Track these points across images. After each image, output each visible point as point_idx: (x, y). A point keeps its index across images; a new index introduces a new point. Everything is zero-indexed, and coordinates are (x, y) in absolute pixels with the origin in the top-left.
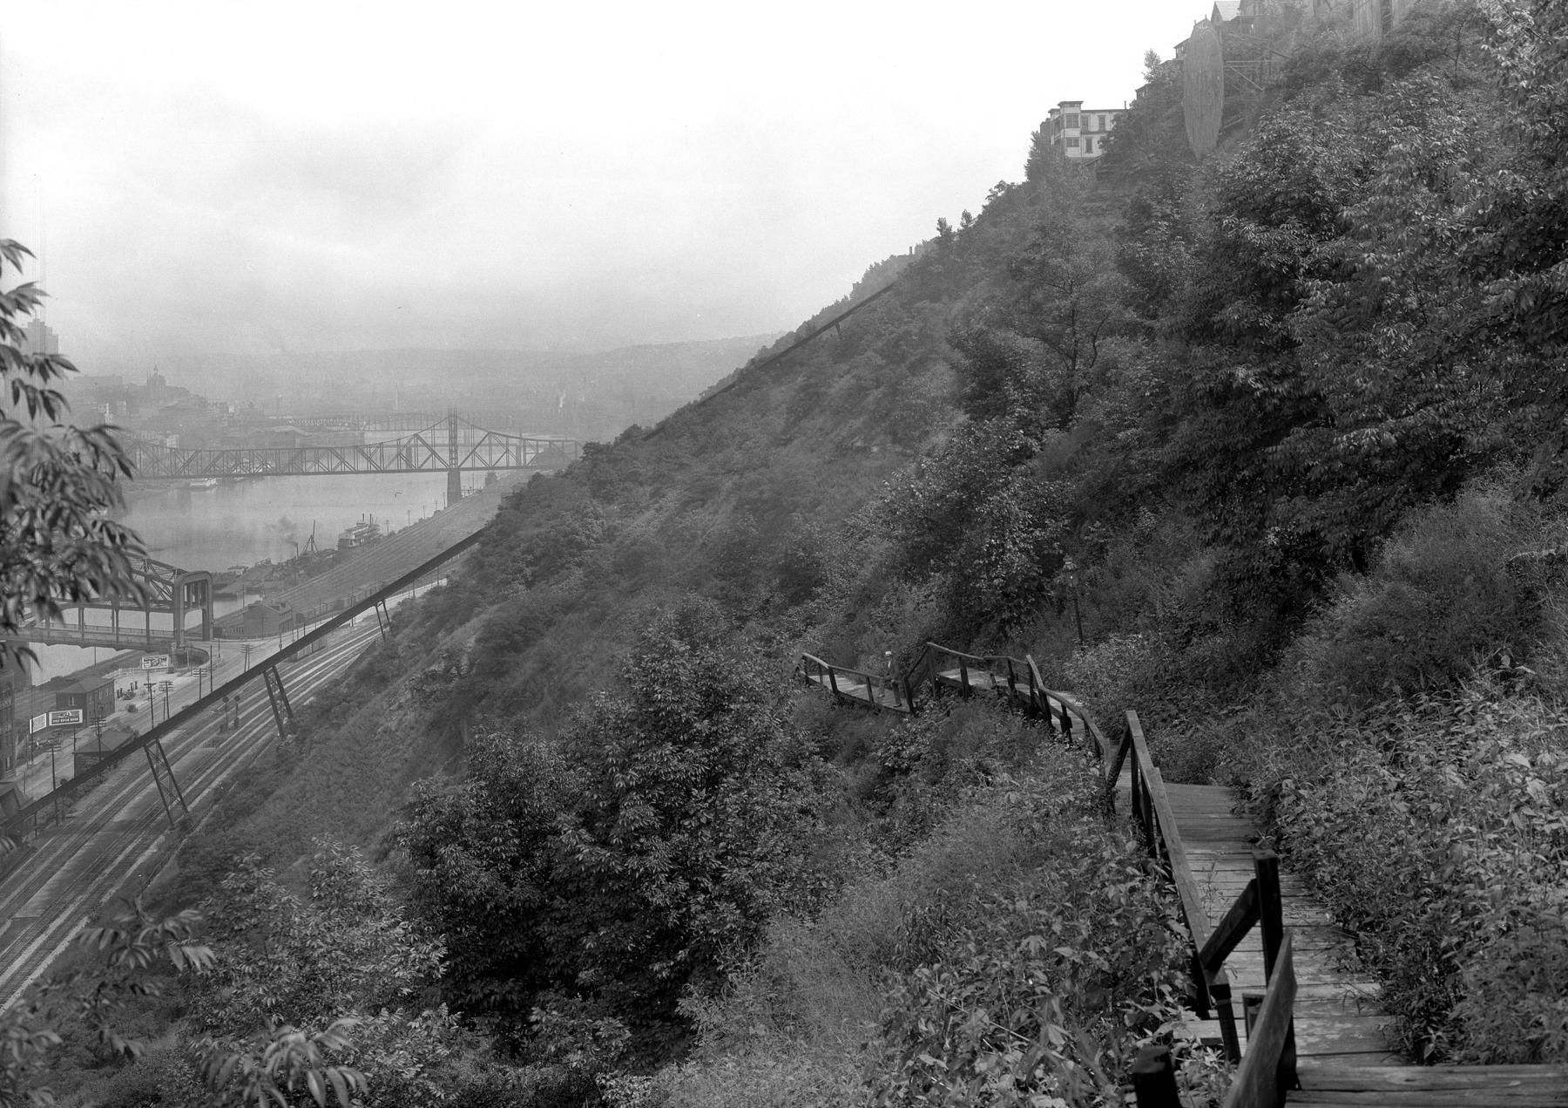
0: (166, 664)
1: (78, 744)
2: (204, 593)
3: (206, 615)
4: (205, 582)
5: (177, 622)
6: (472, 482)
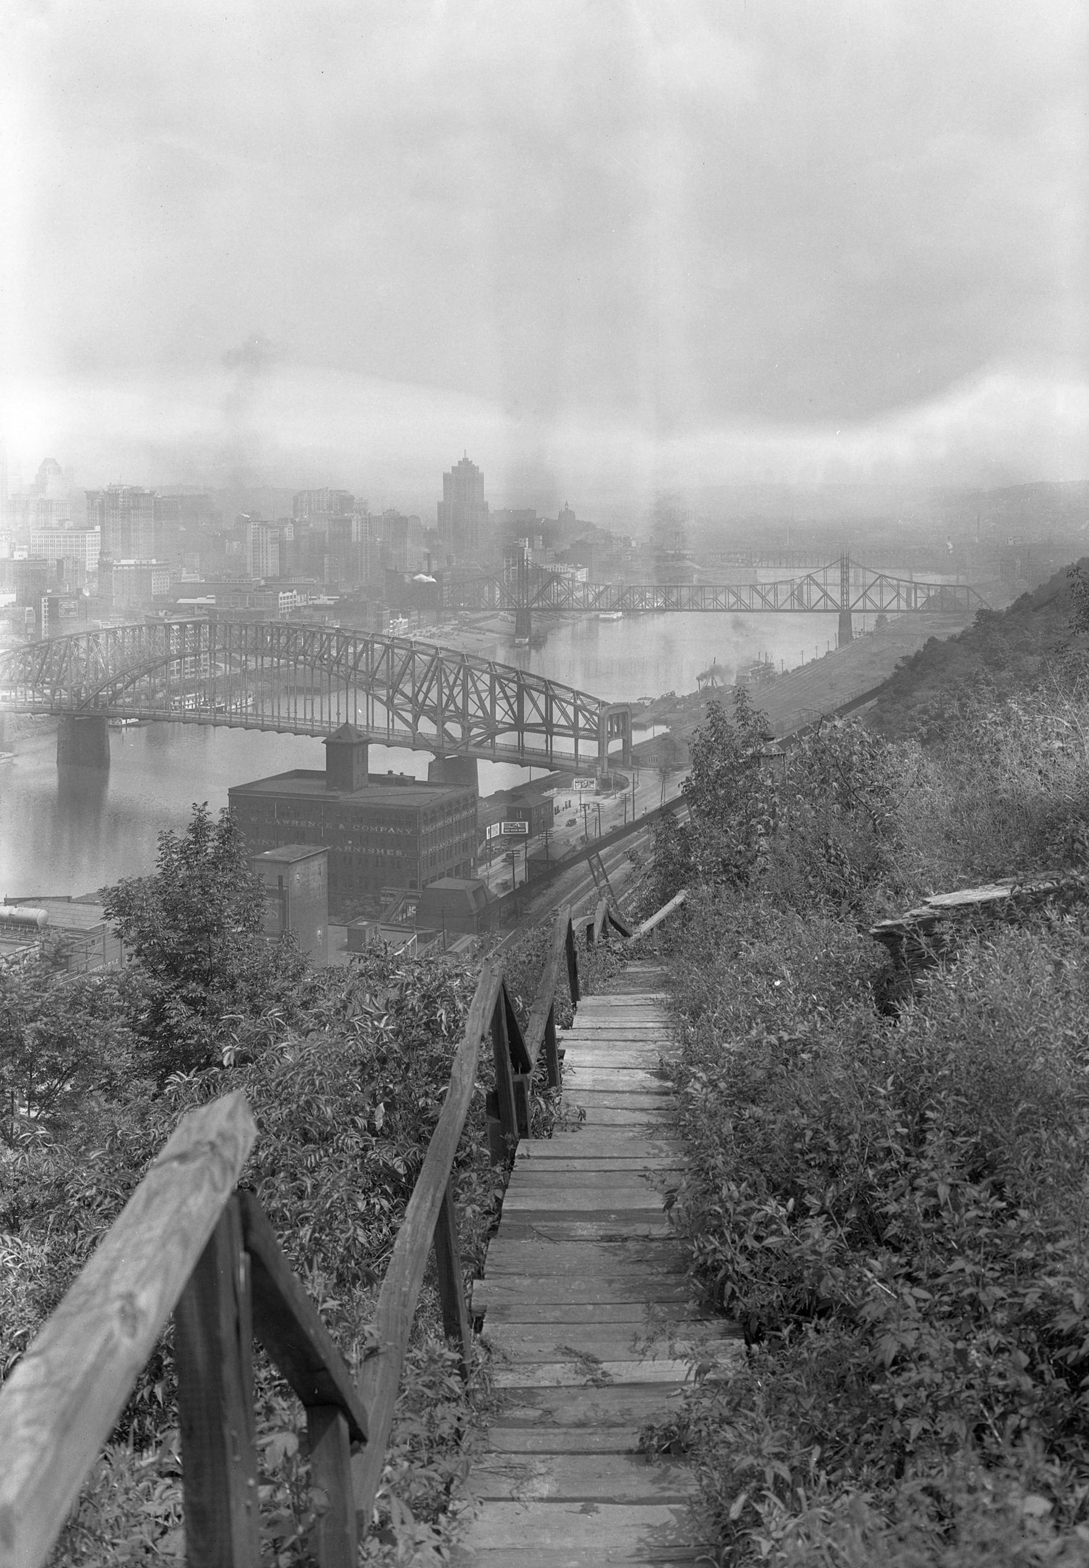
0: (594, 786)
1: (530, 851)
2: (624, 724)
3: (627, 742)
4: (625, 714)
5: (602, 748)
6: (863, 624)
